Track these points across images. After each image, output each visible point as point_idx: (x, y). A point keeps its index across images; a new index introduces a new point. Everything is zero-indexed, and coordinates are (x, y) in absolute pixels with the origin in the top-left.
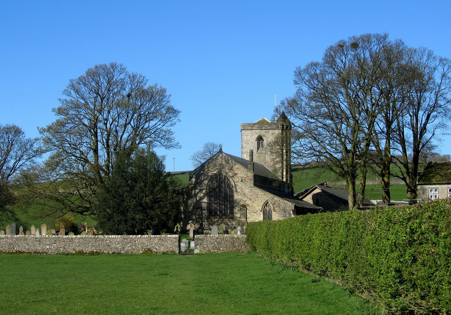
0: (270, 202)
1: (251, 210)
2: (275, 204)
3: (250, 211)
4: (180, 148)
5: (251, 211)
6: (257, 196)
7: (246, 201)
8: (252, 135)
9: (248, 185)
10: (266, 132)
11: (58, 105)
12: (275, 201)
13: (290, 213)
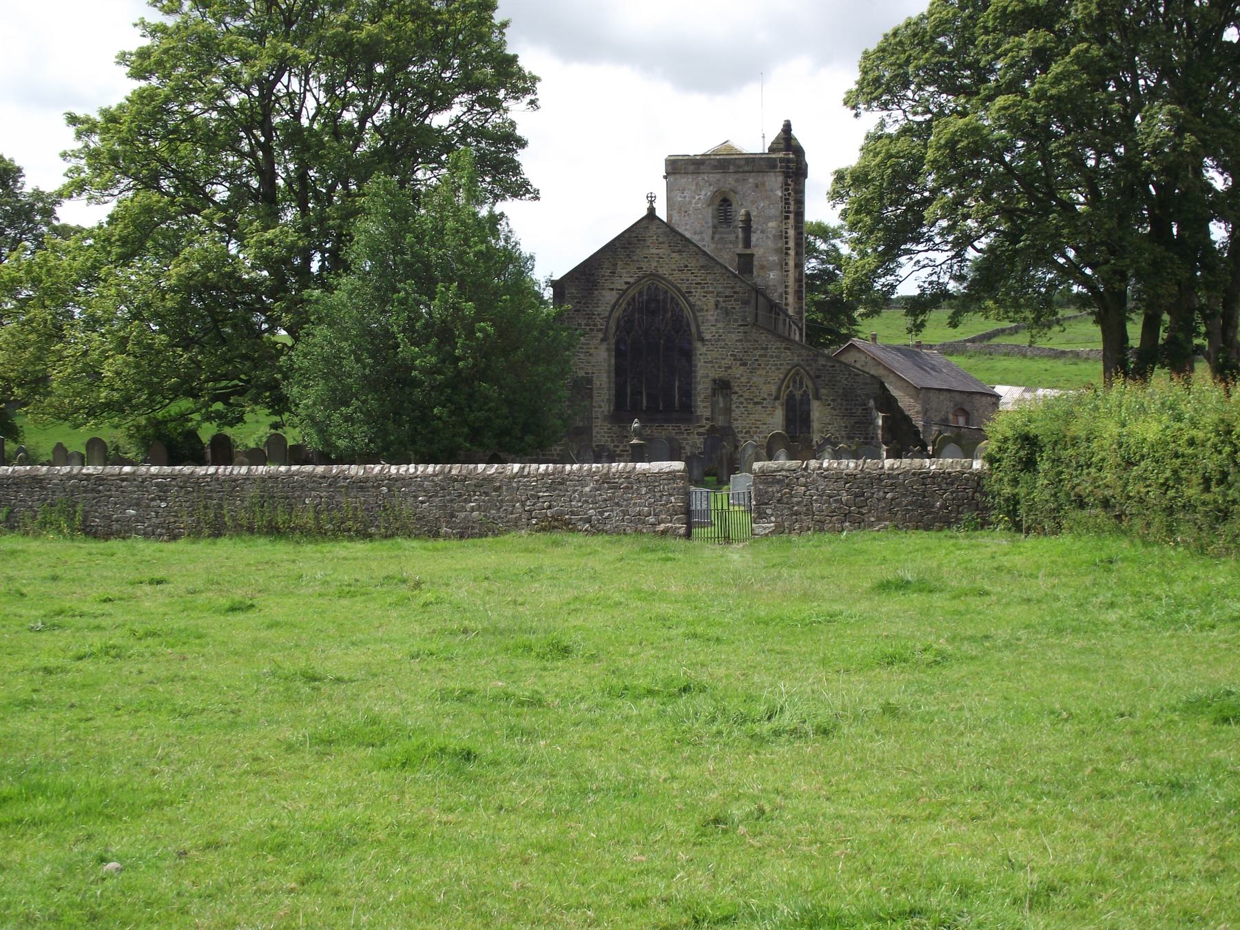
0: (804, 369)
1: (746, 395)
2: (818, 377)
3: (742, 399)
4: (537, 198)
5: (746, 399)
6: (762, 352)
7: (730, 368)
8: (699, 188)
9: (735, 320)
10: (736, 181)
11: (136, 41)
12: (819, 370)
13: (865, 405)
